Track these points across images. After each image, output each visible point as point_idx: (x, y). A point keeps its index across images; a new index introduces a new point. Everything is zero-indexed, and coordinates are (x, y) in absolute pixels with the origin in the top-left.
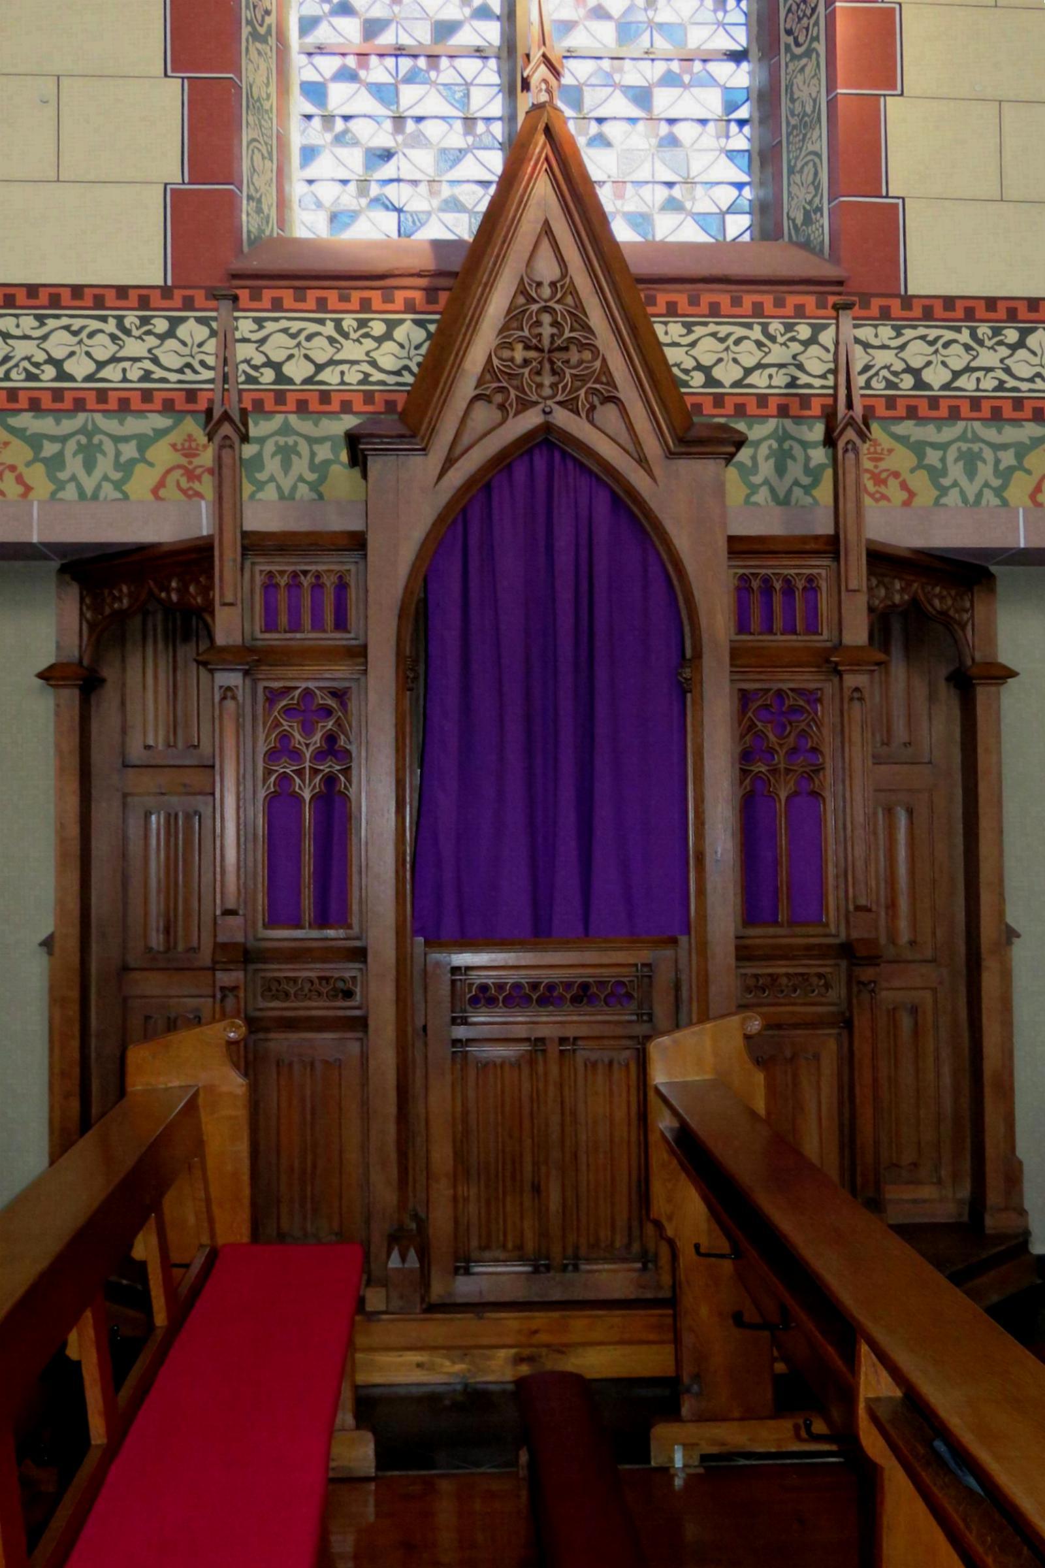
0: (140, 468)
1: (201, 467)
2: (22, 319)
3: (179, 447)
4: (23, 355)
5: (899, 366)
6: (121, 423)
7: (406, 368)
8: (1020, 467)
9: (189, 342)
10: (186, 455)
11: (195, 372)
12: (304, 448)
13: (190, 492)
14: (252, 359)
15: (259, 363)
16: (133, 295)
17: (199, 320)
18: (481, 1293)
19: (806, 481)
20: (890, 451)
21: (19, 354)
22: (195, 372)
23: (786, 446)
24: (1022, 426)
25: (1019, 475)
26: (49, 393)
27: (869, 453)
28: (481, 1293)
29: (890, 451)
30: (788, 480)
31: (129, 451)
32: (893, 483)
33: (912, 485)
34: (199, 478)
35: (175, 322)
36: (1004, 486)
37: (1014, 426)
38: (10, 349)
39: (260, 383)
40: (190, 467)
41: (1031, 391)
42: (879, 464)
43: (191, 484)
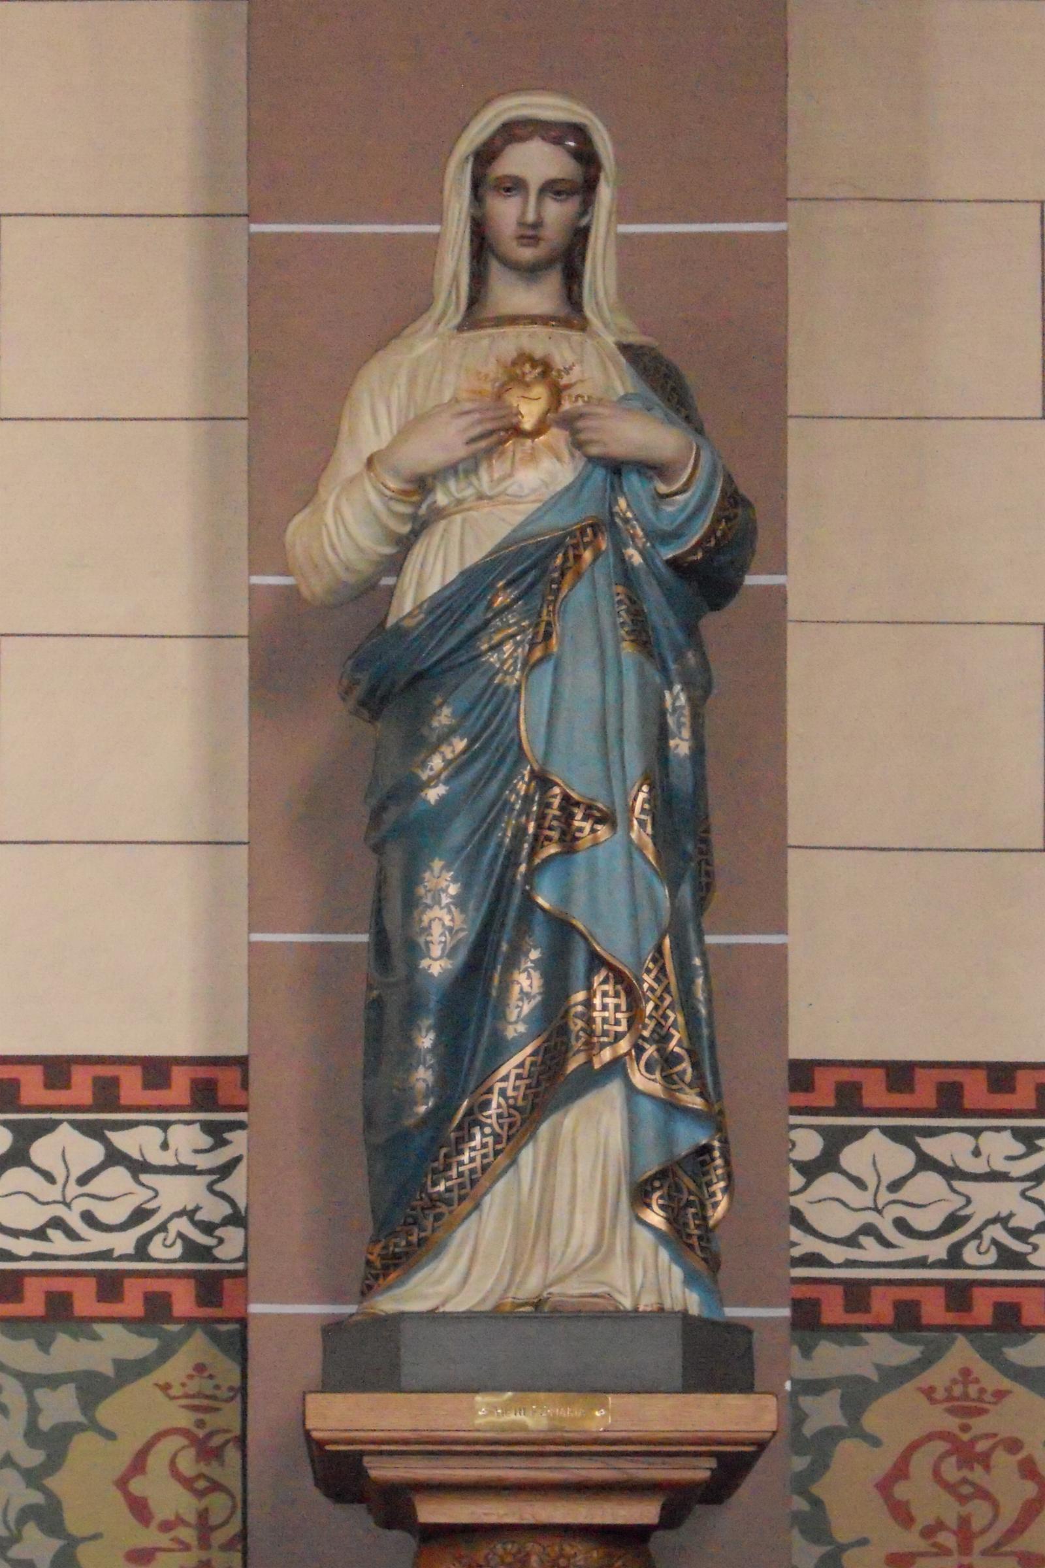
0: (83, 1445)
1: (987, 1436)
2: (986, 1136)
3: (940, 1394)
4: (992, 1215)
5: (215, 1210)
6: (45, 1346)
7: (57, 1223)
8: (855, 1429)
9: (59, 1173)
10: (952, 1411)
11: (72, 1235)
13: (966, 1490)
14: (1011, 1215)
15: (217, 1219)
16: (181, 1079)
17: (897, 1135)
20: (1000, 1395)
21: (980, 1211)
22: (72, 1235)
24: (860, 1342)
25: (847, 1446)
26: (941, 1290)
27: (950, 1398)
29: (1000, 1395)
34: (985, 1459)
35: (836, 1140)
36: (54, 1463)
37: (840, 1344)
38: (959, 1201)
39: (216, 1260)
41: (36, 1257)
43: (965, 1473)
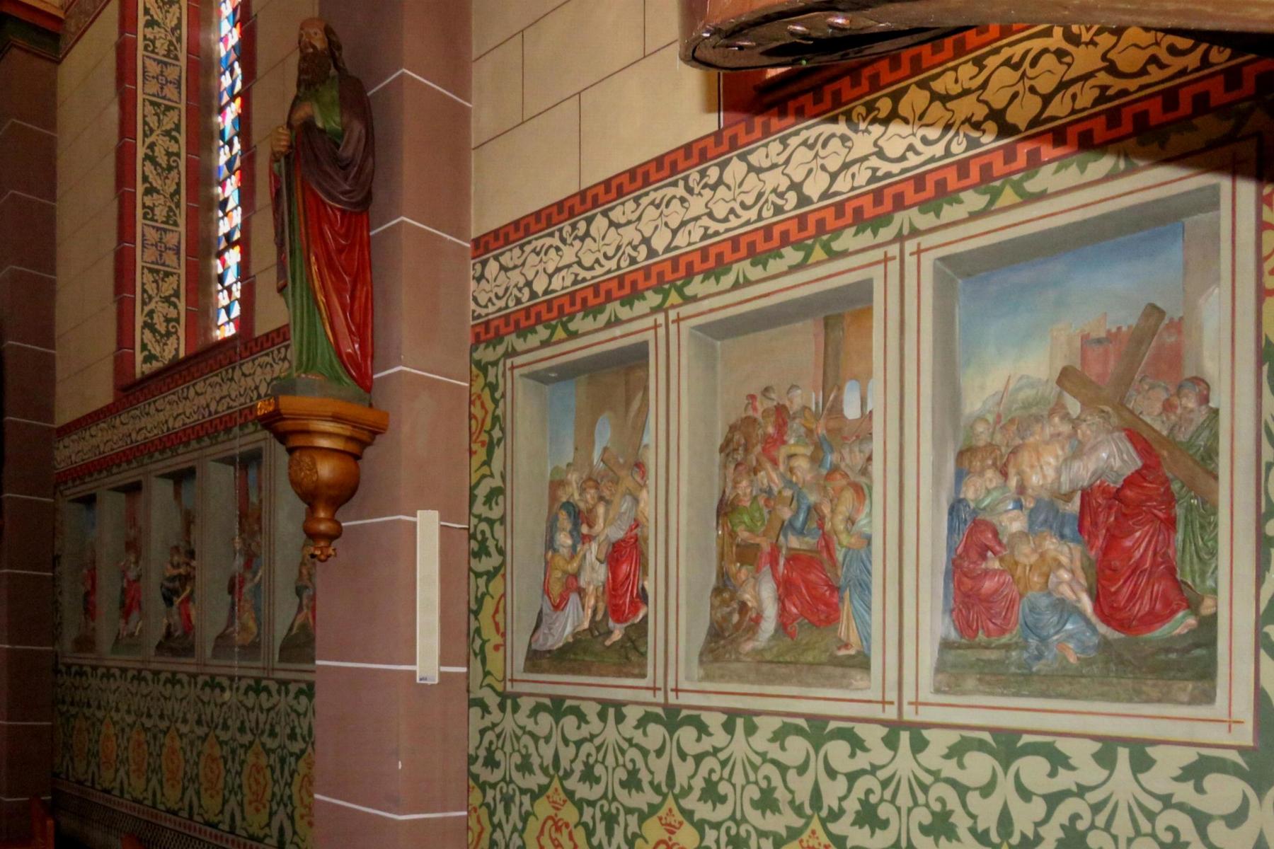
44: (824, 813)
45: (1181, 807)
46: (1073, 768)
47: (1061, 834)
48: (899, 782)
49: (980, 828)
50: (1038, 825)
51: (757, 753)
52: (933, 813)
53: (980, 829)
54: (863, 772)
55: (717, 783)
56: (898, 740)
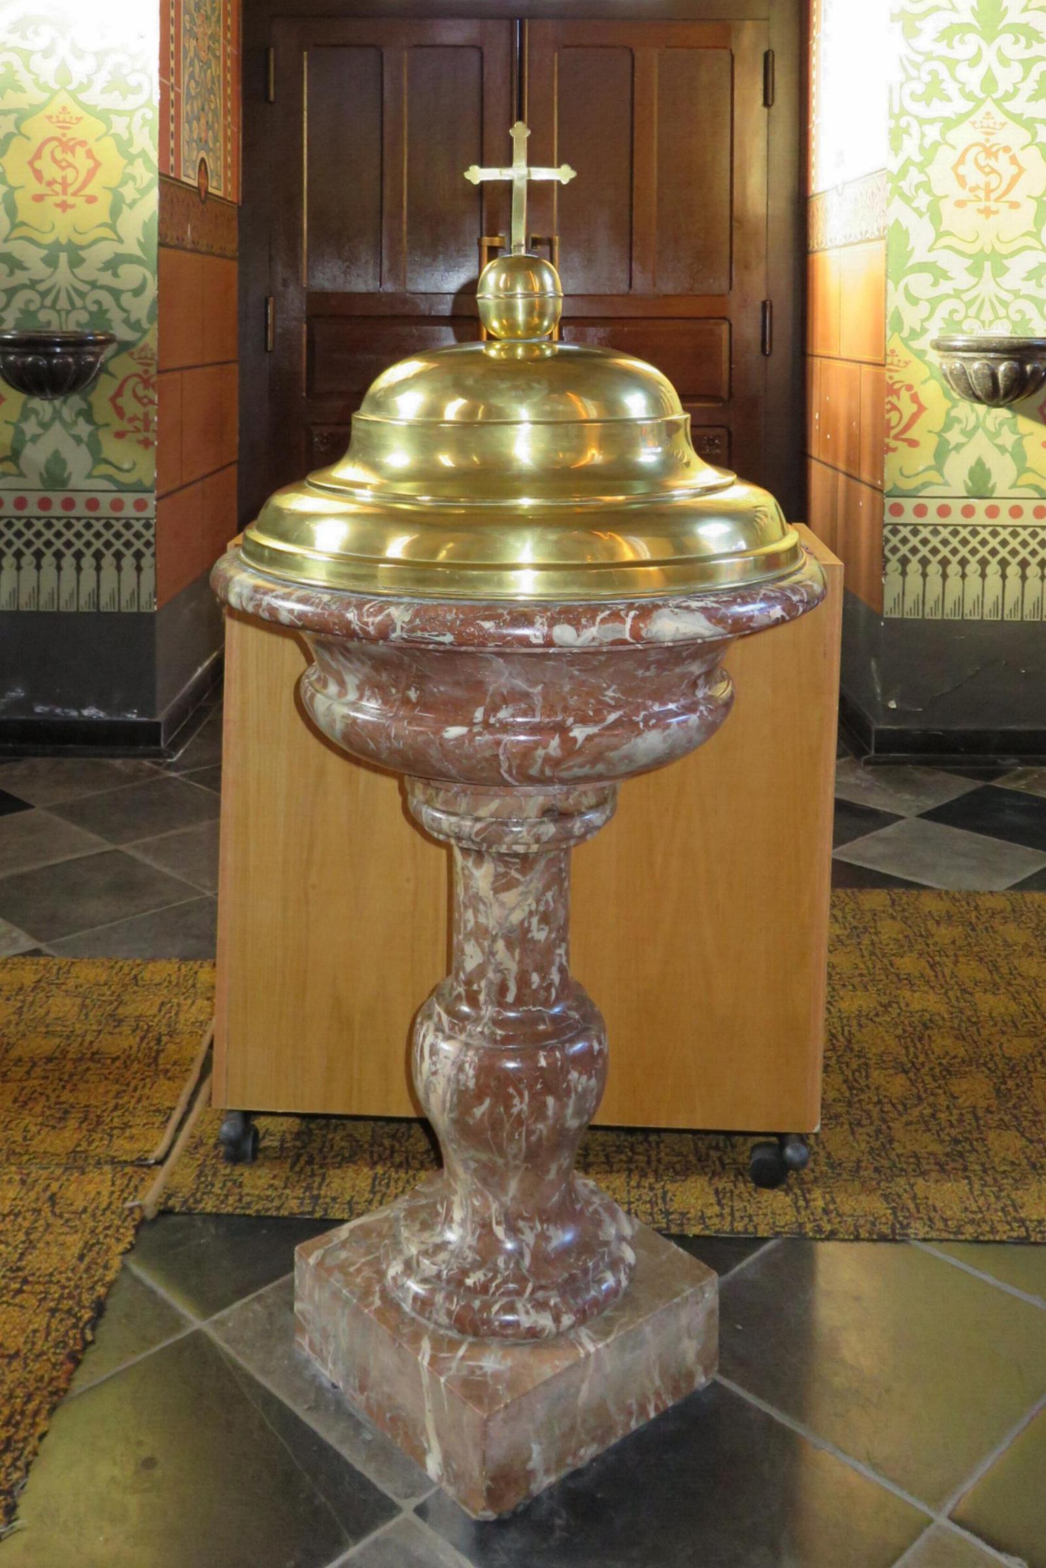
12: (915, 129)
18: (825, 250)
19: (918, 158)
23: (903, 123)
28: (825, 250)
30: (902, 157)
31: (933, 133)
32: (1003, 157)
33: (1021, 157)
40: (988, 145)
42: (991, 137)
44: (905, 333)
45: (102, 287)
46: (25, 269)
47: (19, 315)
48: (983, 301)
49: (133, 318)
50: (923, 321)
51: (83, 281)
52: (91, 313)
53: (132, 320)
54: (24, 286)
55: (36, 312)
56: (982, 269)
